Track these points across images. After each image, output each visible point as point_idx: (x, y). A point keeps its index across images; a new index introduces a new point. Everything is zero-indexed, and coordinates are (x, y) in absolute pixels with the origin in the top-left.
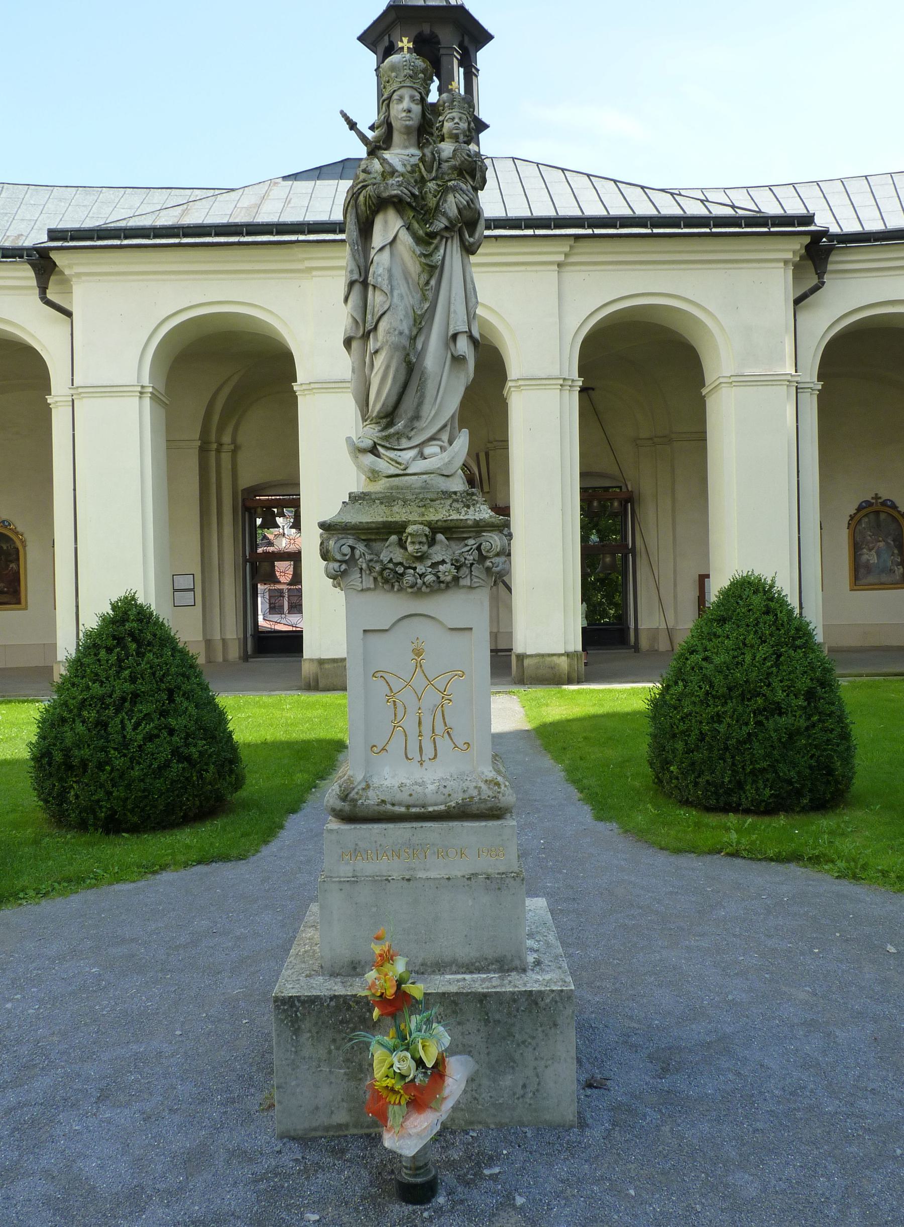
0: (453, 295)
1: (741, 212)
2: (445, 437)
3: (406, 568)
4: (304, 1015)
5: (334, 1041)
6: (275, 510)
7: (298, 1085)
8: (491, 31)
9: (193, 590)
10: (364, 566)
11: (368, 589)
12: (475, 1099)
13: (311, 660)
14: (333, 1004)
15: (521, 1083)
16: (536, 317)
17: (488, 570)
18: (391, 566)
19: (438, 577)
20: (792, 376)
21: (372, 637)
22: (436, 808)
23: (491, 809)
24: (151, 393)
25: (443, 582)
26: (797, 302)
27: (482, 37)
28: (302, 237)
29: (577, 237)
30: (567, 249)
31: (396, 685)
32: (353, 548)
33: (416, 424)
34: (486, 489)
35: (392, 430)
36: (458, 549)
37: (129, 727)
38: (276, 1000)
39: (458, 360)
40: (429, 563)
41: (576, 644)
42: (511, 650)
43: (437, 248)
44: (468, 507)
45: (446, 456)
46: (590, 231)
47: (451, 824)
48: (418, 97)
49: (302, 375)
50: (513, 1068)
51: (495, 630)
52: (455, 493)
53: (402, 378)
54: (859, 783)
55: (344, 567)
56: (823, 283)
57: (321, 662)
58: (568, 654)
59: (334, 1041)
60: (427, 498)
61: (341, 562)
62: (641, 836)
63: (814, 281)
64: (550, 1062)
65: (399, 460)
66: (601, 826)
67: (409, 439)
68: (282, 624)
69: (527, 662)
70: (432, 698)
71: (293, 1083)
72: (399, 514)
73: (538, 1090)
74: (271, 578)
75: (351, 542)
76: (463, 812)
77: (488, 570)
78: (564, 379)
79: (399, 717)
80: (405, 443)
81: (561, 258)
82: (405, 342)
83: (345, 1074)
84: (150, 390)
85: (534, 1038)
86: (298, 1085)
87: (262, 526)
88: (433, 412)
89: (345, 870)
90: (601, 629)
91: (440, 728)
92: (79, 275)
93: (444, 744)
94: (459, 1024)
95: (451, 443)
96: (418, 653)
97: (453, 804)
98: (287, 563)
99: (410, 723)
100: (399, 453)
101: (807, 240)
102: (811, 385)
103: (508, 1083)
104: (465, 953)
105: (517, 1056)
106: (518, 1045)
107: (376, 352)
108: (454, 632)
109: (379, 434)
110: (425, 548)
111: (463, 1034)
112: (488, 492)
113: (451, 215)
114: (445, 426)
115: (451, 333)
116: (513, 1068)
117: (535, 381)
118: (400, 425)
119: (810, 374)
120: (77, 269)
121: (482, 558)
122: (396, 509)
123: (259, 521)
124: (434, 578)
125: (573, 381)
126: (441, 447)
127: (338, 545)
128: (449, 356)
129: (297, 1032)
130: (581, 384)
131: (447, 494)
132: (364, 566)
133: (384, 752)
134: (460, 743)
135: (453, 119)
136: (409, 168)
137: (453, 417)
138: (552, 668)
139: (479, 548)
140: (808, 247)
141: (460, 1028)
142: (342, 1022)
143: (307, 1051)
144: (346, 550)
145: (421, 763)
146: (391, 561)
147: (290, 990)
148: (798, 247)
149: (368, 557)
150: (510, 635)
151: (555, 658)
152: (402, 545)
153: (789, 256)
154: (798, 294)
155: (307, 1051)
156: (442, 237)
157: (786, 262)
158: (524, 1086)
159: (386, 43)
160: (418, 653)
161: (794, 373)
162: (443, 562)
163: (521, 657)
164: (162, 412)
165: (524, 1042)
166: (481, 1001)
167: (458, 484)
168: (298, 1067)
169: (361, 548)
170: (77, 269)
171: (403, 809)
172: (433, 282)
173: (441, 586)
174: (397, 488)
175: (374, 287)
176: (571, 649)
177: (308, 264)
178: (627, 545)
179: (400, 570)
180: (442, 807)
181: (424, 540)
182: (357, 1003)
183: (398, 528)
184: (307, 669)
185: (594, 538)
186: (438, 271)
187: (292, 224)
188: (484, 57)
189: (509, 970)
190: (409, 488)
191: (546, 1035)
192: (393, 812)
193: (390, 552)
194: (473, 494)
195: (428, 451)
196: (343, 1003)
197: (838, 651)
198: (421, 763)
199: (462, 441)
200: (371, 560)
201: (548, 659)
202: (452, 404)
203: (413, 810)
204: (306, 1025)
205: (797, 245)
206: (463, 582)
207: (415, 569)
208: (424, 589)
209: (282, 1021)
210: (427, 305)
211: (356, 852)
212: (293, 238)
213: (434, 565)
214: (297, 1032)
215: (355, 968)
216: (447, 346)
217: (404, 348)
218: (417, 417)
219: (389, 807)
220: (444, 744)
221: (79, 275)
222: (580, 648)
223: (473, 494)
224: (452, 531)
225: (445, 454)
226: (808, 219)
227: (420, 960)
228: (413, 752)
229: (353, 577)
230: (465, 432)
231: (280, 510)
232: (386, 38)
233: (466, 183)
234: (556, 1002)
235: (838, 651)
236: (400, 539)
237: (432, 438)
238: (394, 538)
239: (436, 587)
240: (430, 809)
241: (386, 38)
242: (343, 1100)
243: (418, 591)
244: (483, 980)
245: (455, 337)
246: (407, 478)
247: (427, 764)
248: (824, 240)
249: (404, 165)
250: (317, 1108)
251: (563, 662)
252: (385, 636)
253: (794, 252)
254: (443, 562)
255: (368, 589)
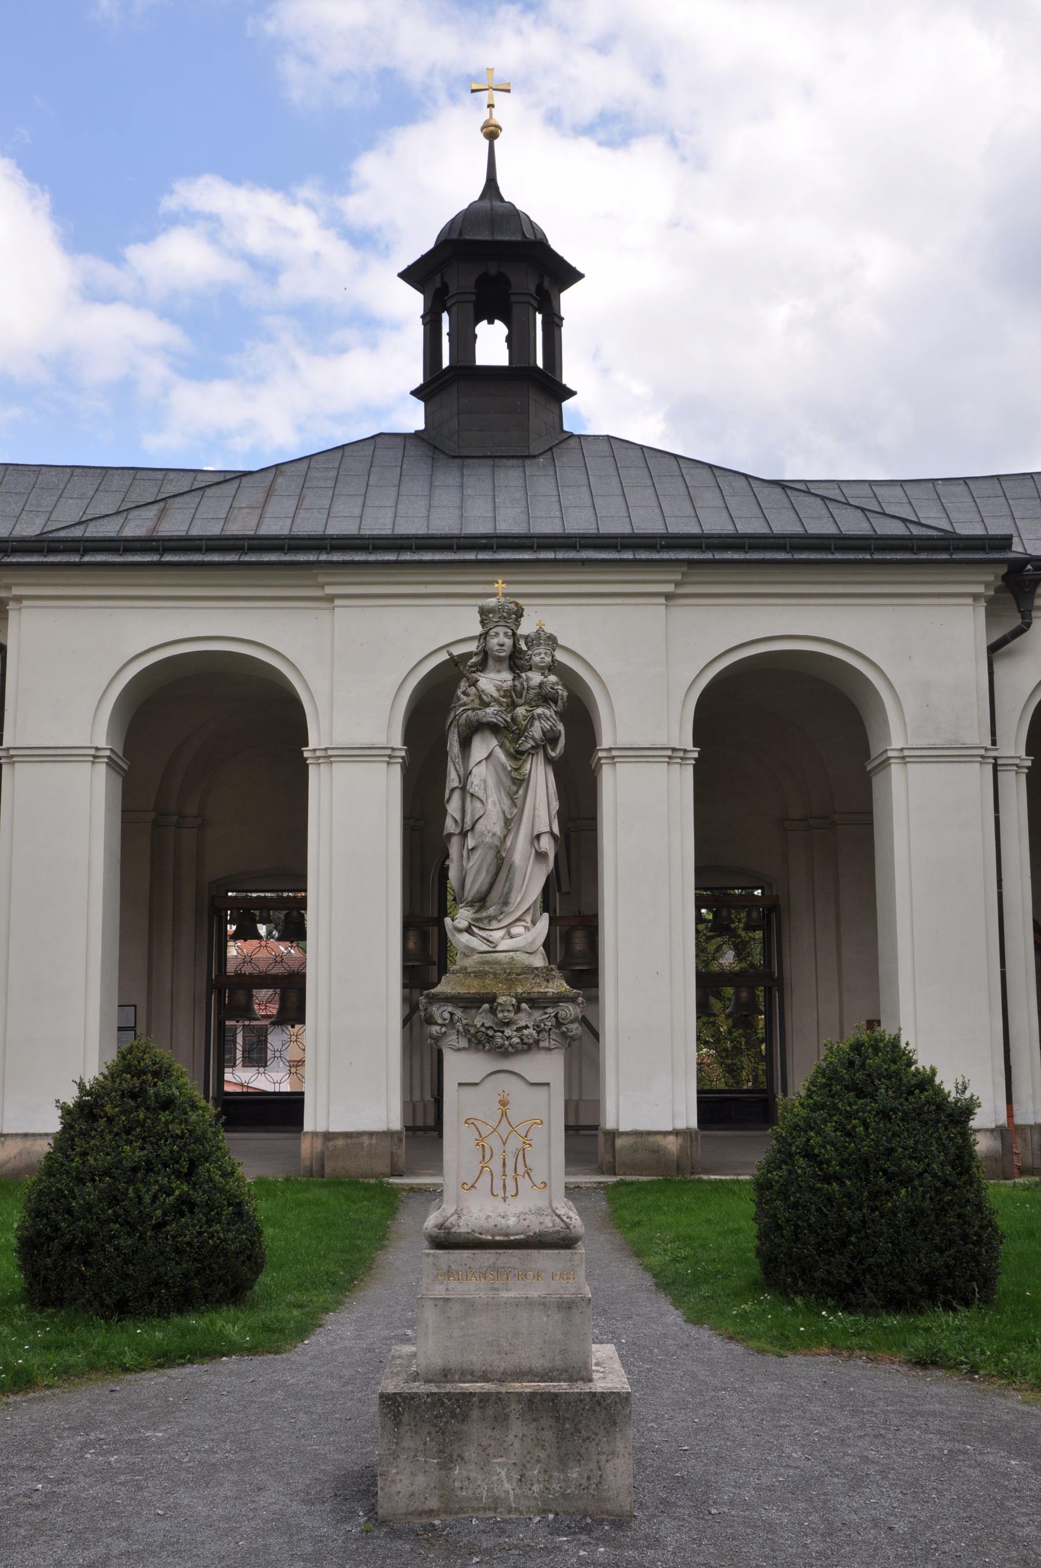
0: (538, 802)
1: (916, 531)
2: (529, 918)
3: (496, 1031)
4: (404, 1410)
5: (429, 1433)
6: (257, 913)
7: (397, 1473)
8: (580, 269)
9: (133, 1029)
10: (461, 1029)
11: (464, 1049)
12: (547, 1489)
13: (315, 1134)
14: (429, 1400)
15: (586, 1476)
16: (646, 665)
17: (564, 1034)
18: (483, 1029)
19: (522, 1040)
20: (986, 749)
21: (464, 1089)
22: (517, 1237)
23: (563, 1239)
24: (108, 757)
25: (525, 1044)
26: (993, 649)
27: (569, 275)
28: (323, 557)
29: (691, 563)
30: (678, 577)
31: (485, 1130)
32: (452, 1014)
33: (505, 909)
34: (565, 888)
35: (484, 914)
36: (538, 1015)
37: (147, 1199)
38: (382, 1396)
39: (541, 856)
40: (515, 1027)
41: (689, 1119)
42: (596, 1128)
43: (525, 761)
44: (548, 981)
45: (529, 936)
46: (709, 556)
47: (529, 1251)
48: (510, 632)
49: (315, 739)
50: (579, 1461)
51: (575, 1097)
52: (537, 969)
53: (493, 870)
54: (1004, 1282)
55: (444, 1029)
56: (1029, 625)
57: (328, 1136)
58: (676, 1133)
59: (429, 1433)
60: (513, 973)
61: (442, 1025)
62: (739, 1333)
63: (1018, 621)
64: (610, 1457)
65: (491, 939)
66: (693, 1330)
67: (499, 921)
68: (270, 1081)
69: (619, 1142)
70: (515, 1143)
71: (394, 1471)
72: (490, 986)
73: (600, 1483)
74: (246, 1011)
75: (450, 1009)
76: (540, 1241)
77: (564, 1034)
78: (674, 750)
79: (486, 1160)
80: (495, 925)
81: (670, 588)
82: (497, 842)
83: (438, 1463)
84: (108, 753)
85: (597, 1434)
86: (397, 1473)
87: (236, 937)
88: (519, 899)
89: (439, 1291)
90: (737, 1099)
91: (521, 1170)
92: (19, 599)
93: (524, 1183)
94: (534, 1420)
95: (534, 923)
96: (504, 1103)
97: (531, 1234)
98: (271, 991)
99: (496, 1165)
100: (490, 933)
101: (1003, 570)
102: (1017, 761)
103: (575, 1475)
104: (538, 1363)
105: (583, 1451)
106: (584, 1441)
107: (473, 849)
108: (535, 1088)
109: (473, 916)
110: (512, 1015)
111: (537, 1429)
112: (568, 893)
113: (537, 736)
114: (529, 909)
115: (535, 833)
116: (579, 1461)
117: (639, 753)
118: (491, 911)
119: (1014, 744)
120: (16, 591)
121: (559, 1024)
122: (487, 981)
123: (232, 928)
124: (518, 1040)
125: (685, 751)
126: (525, 927)
127: (440, 1011)
128: (533, 851)
129: (398, 1424)
130: (696, 755)
131: (532, 970)
132: (461, 1029)
133: (473, 1189)
134: (538, 1183)
135: (540, 654)
136: (502, 693)
137: (535, 901)
138: (656, 1150)
139: (556, 1016)
140: (1004, 578)
141: (535, 1423)
142: (436, 1417)
143: (408, 1443)
144: (446, 1015)
145: (505, 1199)
146: (483, 1025)
147: (391, 1389)
148: (991, 578)
149: (464, 1021)
150: (597, 1106)
151: (659, 1139)
152: (493, 1011)
153: (980, 589)
154: (997, 636)
155: (408, 1443)
156: (529, 754)
157: (976, 597)
158: (589, 1478)
159: (438, 285)
160: (504, 1103)
161: (989, 746)
162: (526, 1027)
163: (613, 1135)
164: (118, 781)
165: (588, 1438)
166: (553, 1401)
167: (539, 961)
168: (398, 1456)
169: (458, 1013)
170: (16, 591)
171: (490, 1237)
172: (521, 792)
173: (528, 1047)
174: (487, 963)
175: (472, 795)
176: (681, 1125)
177: (329, 590)
178: (771, 974)
179: (491, 1033)
180: (522, 1236)
181: (511, 1008)
182: (450, 1400)
183: (492, 999)
184: (306, 1147)
185: (728, 959)
186: (524, 785)
187: (310, 538)
188: (569, 300)
189: (576, 1381)
190: (498, 962)
191: (608, 1432)
192: (480, 1239)
193: (481, 1019)
194: (552, 970)
195: (514, 930)
196: (437, 1399)
197: (330, 1048)
198: (505, 1199)
199: (544, 921)
200: (467, 1025)
201: (651, 1139)
202: (535, 891)
203: (497, 1238)
204: (405, 1418)
205: (992, 576)
206: (542, 1044)
207: (503, 1032)
208: (510, 1049)
209: (386, 1415)
210: (516, 811)
211: (449, 1273)
212: (312, 557)
213: (519, 1029)
214: (398, 1424)
215: (446, 1376)
216: (532, 844)
217: (497, 846)
218: (506, 903)
219: (477, 1235)
220: (524, 1183)
221: (19, 599)
222: (693, 1123)
223: (552, 970)
224: (536, 1002)
225: (529, 934)
226: (1004, 542)
227: (501, 1369)
228: (498, 1189)
229: (451, 1038)
230: (546, 915)
231: (265, 914)
232: (438, 278)
233: (548, 708)
234: (616, 1403)
235: (330, 1048)
236: (491, 1008)
237: (518, 920)
238: (486, 1006)
239: (520, 1047)
240: (512, 1238)
241: (438, 278)
242: (435, 1487)
243: (504, 1052)
244: (554, 1386)
245: (538, 837)
246: (496, 954)
247: (510, 1200)
248: (1029, 567)
249: (498, 690)
250: (413, 1494)
251: (672, 1144)
252: (473, 1088)
253: (987, 585)
254: (526, 1027)
255: (464, 1049)
